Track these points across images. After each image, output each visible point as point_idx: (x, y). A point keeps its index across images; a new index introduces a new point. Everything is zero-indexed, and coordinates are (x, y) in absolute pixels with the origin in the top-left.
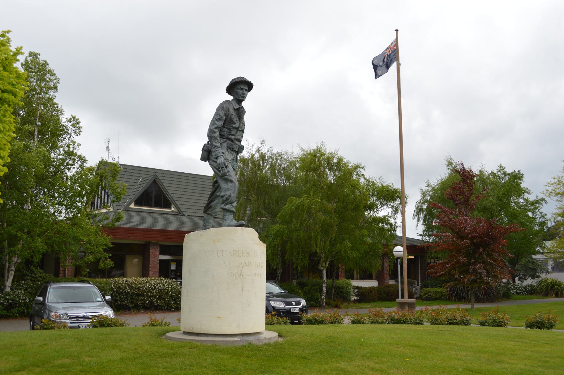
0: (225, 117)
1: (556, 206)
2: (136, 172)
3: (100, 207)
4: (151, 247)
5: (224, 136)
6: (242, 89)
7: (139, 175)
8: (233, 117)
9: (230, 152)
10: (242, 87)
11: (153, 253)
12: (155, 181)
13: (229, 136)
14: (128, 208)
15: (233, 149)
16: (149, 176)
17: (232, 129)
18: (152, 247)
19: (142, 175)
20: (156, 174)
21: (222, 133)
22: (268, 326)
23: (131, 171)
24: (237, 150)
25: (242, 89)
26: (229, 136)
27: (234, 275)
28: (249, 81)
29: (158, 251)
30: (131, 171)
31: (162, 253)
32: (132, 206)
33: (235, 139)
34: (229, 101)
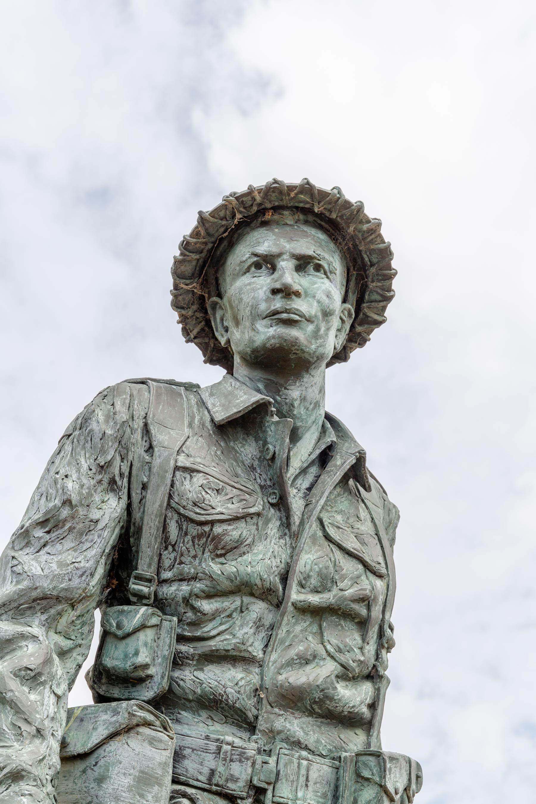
17: (207, 606)
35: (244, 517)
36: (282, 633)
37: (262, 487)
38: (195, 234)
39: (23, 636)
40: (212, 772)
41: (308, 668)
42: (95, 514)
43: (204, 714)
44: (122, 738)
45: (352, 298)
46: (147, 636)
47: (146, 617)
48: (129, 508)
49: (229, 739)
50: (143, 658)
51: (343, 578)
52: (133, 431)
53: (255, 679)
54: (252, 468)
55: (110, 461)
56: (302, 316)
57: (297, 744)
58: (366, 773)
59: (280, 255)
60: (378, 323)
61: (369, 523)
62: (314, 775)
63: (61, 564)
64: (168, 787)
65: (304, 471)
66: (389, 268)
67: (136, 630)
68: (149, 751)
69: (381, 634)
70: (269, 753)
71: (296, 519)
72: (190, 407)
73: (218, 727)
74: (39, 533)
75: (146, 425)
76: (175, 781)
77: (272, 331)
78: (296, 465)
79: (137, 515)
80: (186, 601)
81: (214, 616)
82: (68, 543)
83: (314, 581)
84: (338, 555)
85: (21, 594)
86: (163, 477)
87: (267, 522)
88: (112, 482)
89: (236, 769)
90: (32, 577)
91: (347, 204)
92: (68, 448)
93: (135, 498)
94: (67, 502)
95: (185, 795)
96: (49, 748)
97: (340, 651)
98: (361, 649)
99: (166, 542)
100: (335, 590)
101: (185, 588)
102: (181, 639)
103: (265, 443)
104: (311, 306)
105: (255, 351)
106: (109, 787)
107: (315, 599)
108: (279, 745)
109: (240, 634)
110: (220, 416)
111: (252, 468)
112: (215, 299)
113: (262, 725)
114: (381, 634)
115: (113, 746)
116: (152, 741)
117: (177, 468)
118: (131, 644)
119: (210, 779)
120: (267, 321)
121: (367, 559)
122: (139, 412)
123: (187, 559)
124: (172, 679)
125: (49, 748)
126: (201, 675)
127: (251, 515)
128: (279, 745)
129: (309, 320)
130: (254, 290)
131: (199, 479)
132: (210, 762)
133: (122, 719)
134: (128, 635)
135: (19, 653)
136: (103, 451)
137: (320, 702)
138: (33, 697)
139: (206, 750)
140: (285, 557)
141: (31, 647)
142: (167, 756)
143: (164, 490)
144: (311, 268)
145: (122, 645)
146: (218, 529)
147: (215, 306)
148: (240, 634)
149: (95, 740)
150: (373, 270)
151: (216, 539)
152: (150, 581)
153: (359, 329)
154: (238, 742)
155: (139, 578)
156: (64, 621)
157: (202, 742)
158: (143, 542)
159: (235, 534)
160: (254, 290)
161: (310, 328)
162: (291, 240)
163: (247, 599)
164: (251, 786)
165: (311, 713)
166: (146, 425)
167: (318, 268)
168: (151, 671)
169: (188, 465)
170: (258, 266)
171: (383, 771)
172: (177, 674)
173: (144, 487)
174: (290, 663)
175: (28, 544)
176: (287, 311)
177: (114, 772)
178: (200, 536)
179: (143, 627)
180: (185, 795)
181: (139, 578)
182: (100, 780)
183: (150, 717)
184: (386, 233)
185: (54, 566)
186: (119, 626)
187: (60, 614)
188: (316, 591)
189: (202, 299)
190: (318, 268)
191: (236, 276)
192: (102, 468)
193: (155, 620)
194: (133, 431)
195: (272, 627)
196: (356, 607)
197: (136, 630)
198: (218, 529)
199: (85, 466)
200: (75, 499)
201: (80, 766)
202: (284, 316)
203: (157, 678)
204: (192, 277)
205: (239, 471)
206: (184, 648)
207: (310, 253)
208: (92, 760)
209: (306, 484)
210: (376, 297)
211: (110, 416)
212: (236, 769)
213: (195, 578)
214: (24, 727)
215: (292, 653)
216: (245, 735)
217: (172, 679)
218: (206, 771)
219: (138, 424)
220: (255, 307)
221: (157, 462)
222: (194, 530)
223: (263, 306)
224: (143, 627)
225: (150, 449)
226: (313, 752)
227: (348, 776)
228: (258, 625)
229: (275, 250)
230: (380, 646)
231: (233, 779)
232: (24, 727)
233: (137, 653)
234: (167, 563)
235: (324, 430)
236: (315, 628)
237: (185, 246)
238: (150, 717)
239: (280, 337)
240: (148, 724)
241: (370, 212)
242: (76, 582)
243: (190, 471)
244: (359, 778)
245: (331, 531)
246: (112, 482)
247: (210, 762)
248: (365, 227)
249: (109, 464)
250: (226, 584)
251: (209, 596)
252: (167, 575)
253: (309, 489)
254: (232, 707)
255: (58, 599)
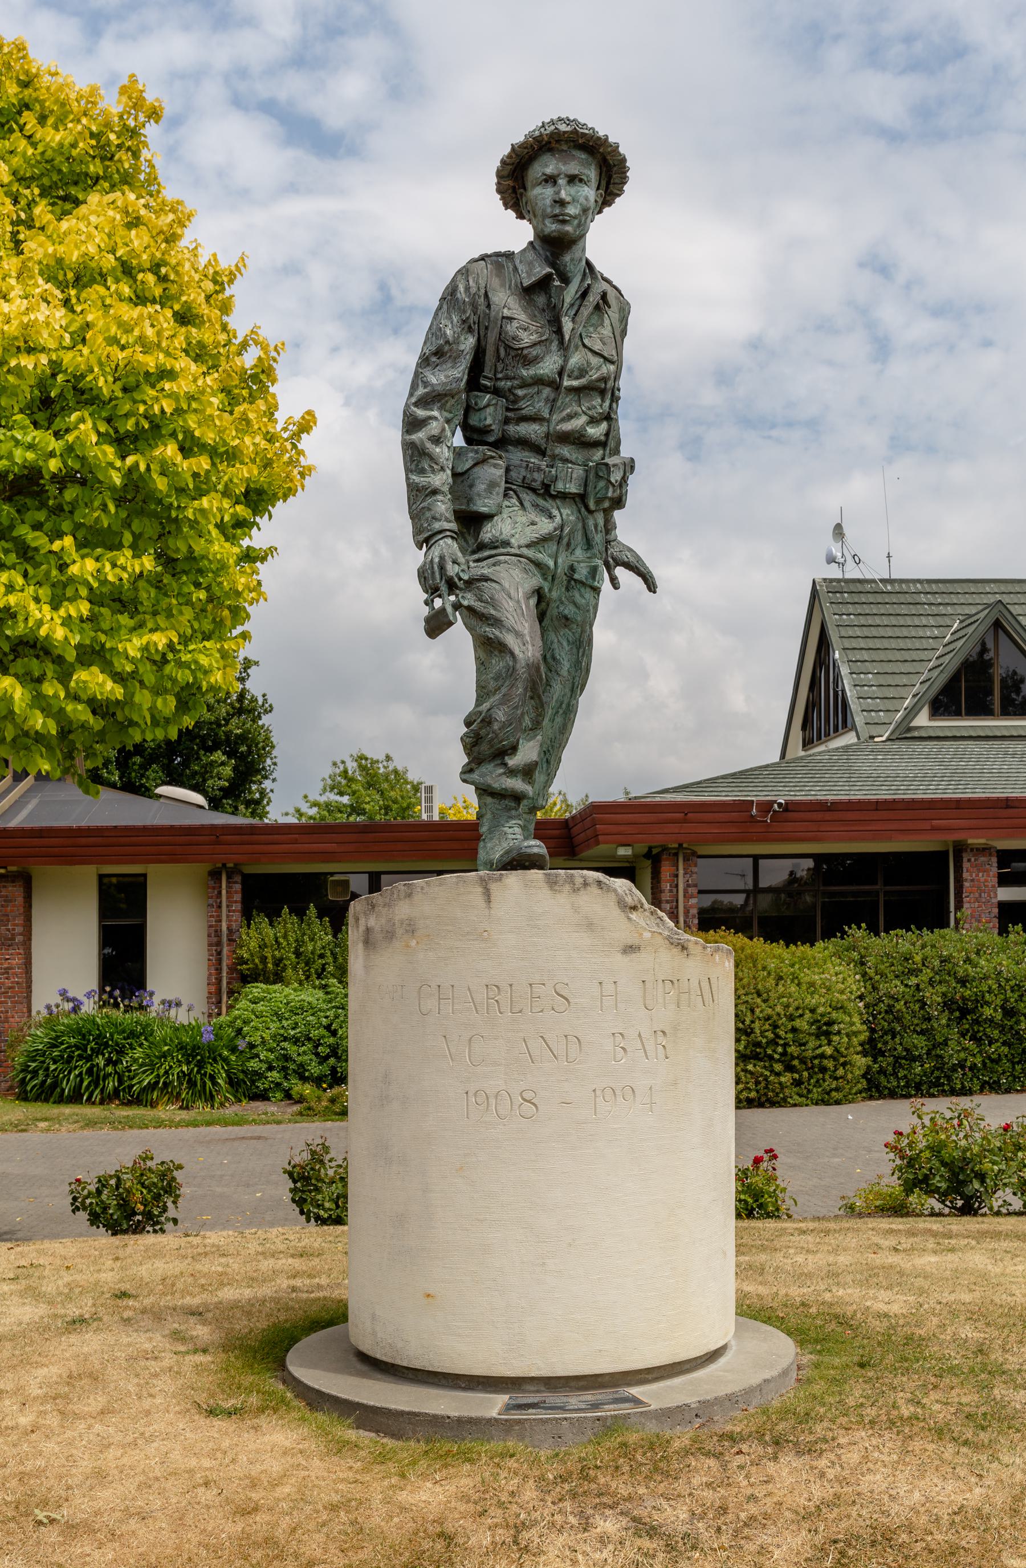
0: (469, 342)
1: (274, 780)
2: (939, 600)
3: (836, 730)
4: (965, 860)
5: (486, 431)
6: (551, 180)
7: (949, 610)
8: (511, 328)
9: (536, 506)
10: (549, 170)
11: (972, 880)
12: (997, 625)
13: (512, 429)
14: (909, 729)
15: (546, 487)
16: (980, 607)
17: (520, 392)
18: (969, 860)
19: (959, 610)
20: (998, 597)
21: (474, 420)
22: (741, 1319)
23: (923, 598)
24: (573, 488)
25: (551, 180)
26: (512, 429)
27: (492, 1101)
28: (601, 134)
29: (994, 870)
30: (923, 598)
31: (1004, 881)
32: (923, 720)
33: (548, 435)
34: (509, 256)
35: (540, 342)
36: (559, 404)
37: (549, 321)
38: (509, 156)
39: (431, 418)
40: (524, 478)
41: (572, 421)
42: (462, 347)
43: (520, 447)
44: (480, 465)
45: (604, 183)
46: (490, 410)
47: (490, 400)
48: (479, 340)
49: (532, 460)
50: (489, 421)
51: (591, 369)
52: (479, 297)
53: (544, 429)
54: (544, 310)
55: (800, 1335)
56: (570, 216)
57: (566, 461)
58: (601, 474)
59: (559, 175)
60: (619, 195)
61: (610, 328)
62: (574, 476)
63: (447, 377)
64: (503, 485)
65: (572, 305)
66: (625, 167)
67: (485, 407)
68: (493, 470)
69: (613, 394)
70: (552, 467)
71: (567, 337)
72: (509, 273)
73: (527, 454)
74: (434, 359)
75: (486, 292)
76: (507, 482)
77: (554, 227)
78: (568, 300)
79: (483, 343)
80: (510, 390)
81: (525, 396)
82: (449, 365)
83: (576, 373)
84: (589, 354)
85: (427, 394)
86: (496, 324)
87: (552, 342)
88: (470, 327)
89: (536, 475)
90: (432, 385)
91: (599, 138)
92: (445, 307)
93: (482, 334)
94: (447, 342)
95: (511, 489)
96: (565, 541)
97: (589, 409)
98: (601, 406)
99: (498, 358)
100: (587, 376)
101: (509, 383)
102: (508, 409)
103: (550, 297)
104: (576, 208)
105: (544, 236)
106: (475, 490)
107: (575, 383)
108: (558, 462)
109: (537, 406)
110: (526, 283)
111: (544, 310)
112: (522, 190)
113: (549, 452)
114: (613, 394)
115: (476, 469)
116: (495, 466)
117: (503, 317)
118: (482, 415)
119: (523, 482)
120: (550, 220)
121: (606, 354)
122: (482, 285)
123: (509, 368)
124: (504, 430)
125: (565, 541)
126: (518, 428)
127: (542, 341)
128: (558, 462)
129: (575, 217)
130: (544, 199)
131: (515, 324)
132: (523, 472)
133: (480, 456)
134: (480, 409)
135: (429, 427)
136: (464, 312)
137: (579, 438)
138: (438, 450)
139: (520, 466)
140: (560, 362)
141: (434, 424)
142: (501, 472)
143: (496, 331)
144: (577, 180)
145: (478, 414)
146: (525, 352)
147: (521, 194)
148: (537, 406)
149: (467, 466)
150: (615, 169)
151: (525, 357)
152: (491, 379)
153: (608, 198)
154: (536, 461)
155: (486, 377)
156: (448, 405)
157: (519, 462)
158: (487, 358)
159: (535, 353)
160: (544, 199)
161: (576, 222)
162: (565, 164)
163: (541, 387)
164: (543, 483)
165: (574, 444)
166: (486, 292)
167: (581, 180)
168: (493, 427)
169: (509, 315)
170: (546, 181)
171: (609, 473)
172: (506, 427)
173: (487, 328)
174: (563, 420)
175: (428, 365)
176: (562, 215)
177: (477, 482)
178: (516, 356)
179: (488, 405)
180: (511, 489)
181: (486, 377)
182: (471, 486)
183: (494, 454)
184: (622, 150)
185: (443, 378)
186: (476, 404)
187: (447, 402)
188: (577, 378)
189: (514, 188)
190: (581, 180)
191: (534, 186)
192: (464, 322)
193: (494, 402)
194: (479, 297)
195: (554, 400)
196: (598, 384)
197: (485, 407)
198: (525, 352)
199: (455, 320)
200: (451, 339)
201: (461, 479)
202: (561, 217)
203: (496, 431)
204: (508, 176)
205: (536, 313)
206: (509, 414)
207: (577, 172)
208: (466, 476)
209: (573, 312)
210: (617, 181)
211: (467, 289)
212: (536, 475)
213: (514, 378)
214: (435, 467)
215: (565, 413)
216: (540, 457)
217: (504, 430)
218: (521, 477)
219: (483, 291)
220: (544, 211)
221: (493, 314)
222: (513, 353)
223: (549, 210)
224: (488, 405)
225: (489, 306)
226: (574, 464)
227: (592, 476)
228: (547, 400)
229: (556, 172)
230: (612, 401)
231: (534, 480)
232: (435, 467)
233: (485, 419)
234: (499, 369)
235: (584, 274)
236: (576, 398)
237: (503, 162)
238: (494, 454)
239: (559, 231)
240: (492, 457)
241: (611, 140)
242: (454, 385)
243: (511, 319)
244: (598, 477)
245: (586, 341)
246: (470, 327)
247: (523, 472)
248: (609, 149)
249: (468, 318)
250: (530, 381)
251: (521, 387)
252: (500, 376)
253: (575, 315)
254: (534, 444)
255: (446, 395)
